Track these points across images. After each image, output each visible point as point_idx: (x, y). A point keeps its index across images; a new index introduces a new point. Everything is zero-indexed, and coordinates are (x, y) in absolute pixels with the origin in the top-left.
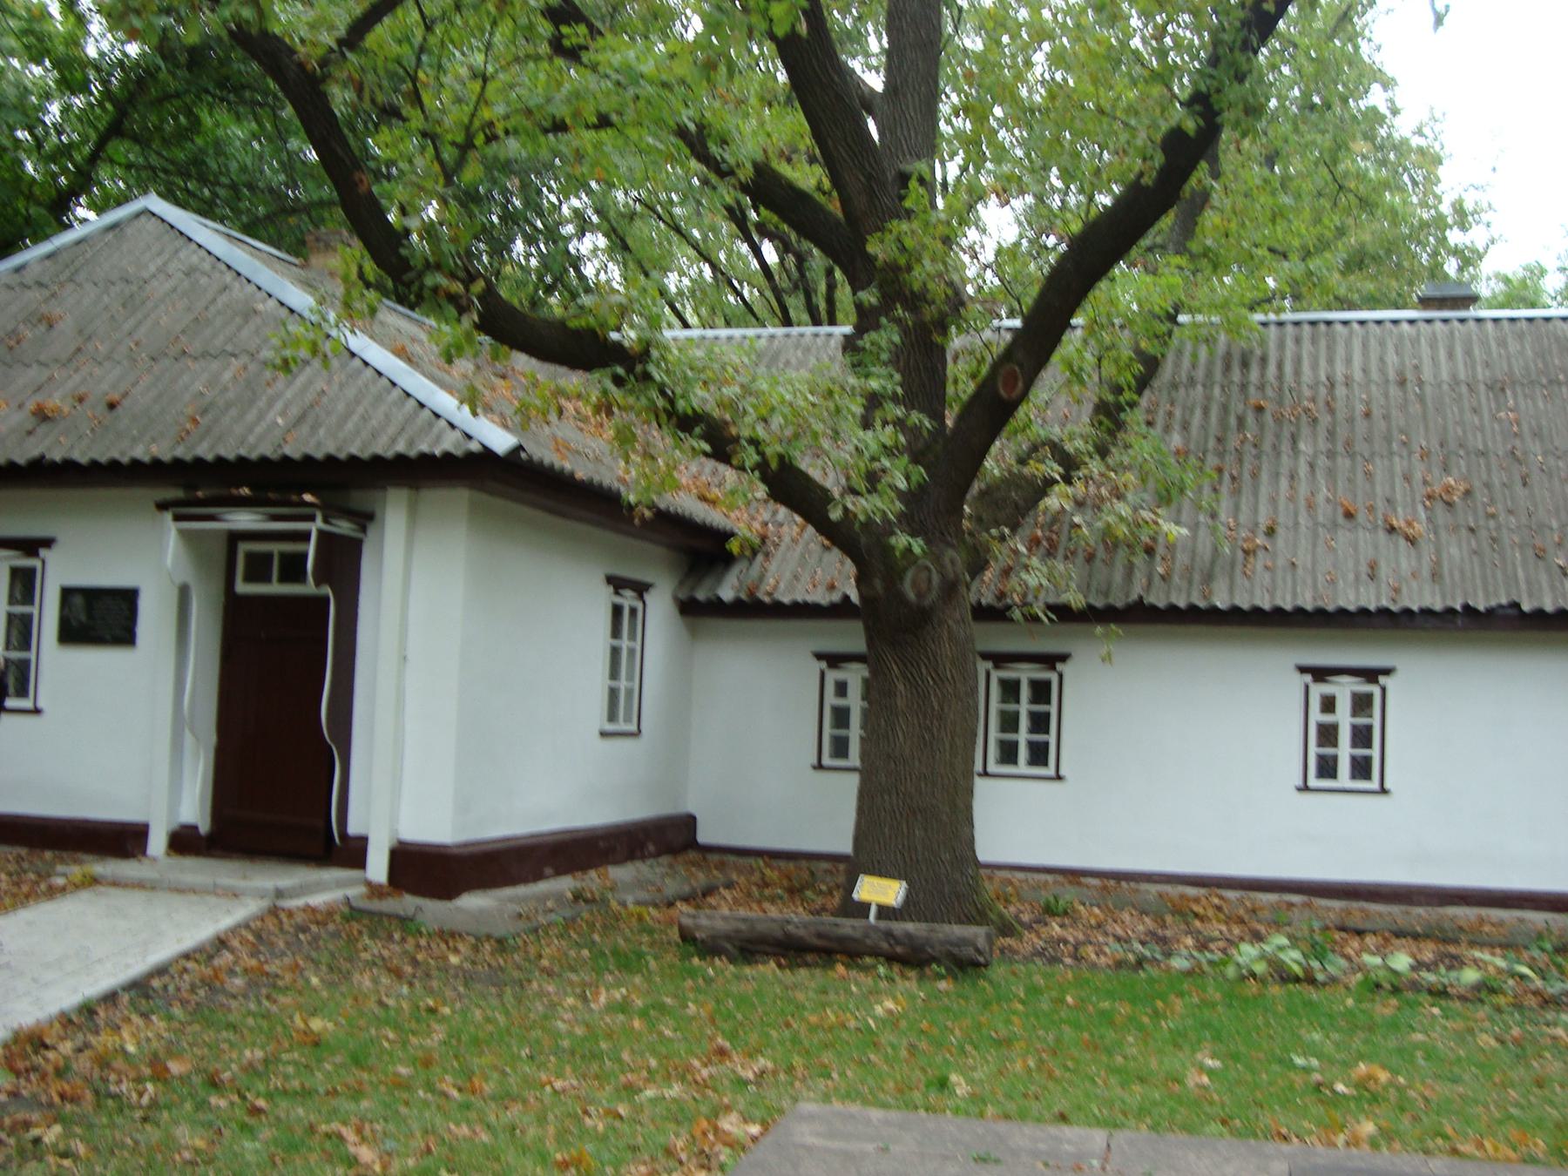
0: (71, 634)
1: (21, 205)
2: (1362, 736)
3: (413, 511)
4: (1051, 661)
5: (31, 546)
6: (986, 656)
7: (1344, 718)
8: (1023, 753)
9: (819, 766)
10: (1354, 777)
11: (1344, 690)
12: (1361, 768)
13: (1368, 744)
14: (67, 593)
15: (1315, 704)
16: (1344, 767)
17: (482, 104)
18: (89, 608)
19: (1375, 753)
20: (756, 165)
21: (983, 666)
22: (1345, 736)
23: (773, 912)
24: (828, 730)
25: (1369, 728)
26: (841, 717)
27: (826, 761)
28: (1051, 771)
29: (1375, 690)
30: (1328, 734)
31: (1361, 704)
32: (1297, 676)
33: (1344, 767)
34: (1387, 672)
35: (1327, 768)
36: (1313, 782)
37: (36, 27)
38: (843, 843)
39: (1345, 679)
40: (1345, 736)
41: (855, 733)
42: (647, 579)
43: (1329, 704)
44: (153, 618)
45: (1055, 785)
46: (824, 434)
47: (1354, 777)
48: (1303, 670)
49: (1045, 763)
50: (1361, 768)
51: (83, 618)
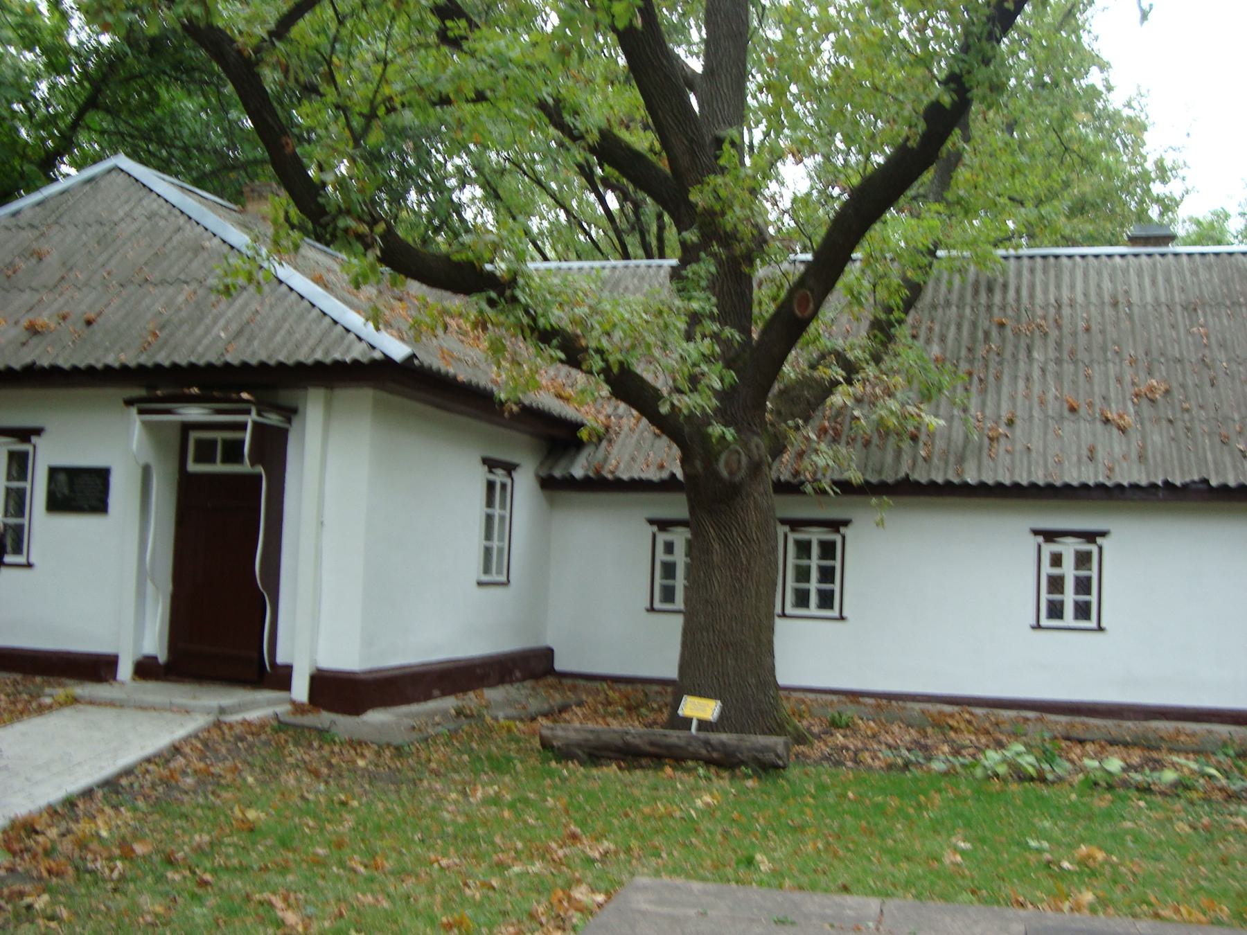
0: (57, 504)
1: (16, 163)
2: (1083, 585)
3: (328, 407)
4: (836, 525)
5: (25, 434)
6: (784, 522)
7: (1069, 571)
8: (814, 599)
9: (652, 609)
10: (1077, 617)
11: (1069, 548)
12: (1083, 611)
13: (1088, 591)
14: (53, 472)
15: (1046, 560)
16: (1069, 610)
17: (383, 83)
18: (71, 483)
19: (1093, 598)
20: (601, 131)
21: (782, 530)
22: (1069, 585)
23: (615, 725)
24: (658, 581)
25: (1089, 579)
26: (669, 570)
27: (657, 605)
28: (836, 613)
29: (1094, 549)
30: (1056, 584)
31: (1083, 560)
32: (1031, 538)
33: (1069, 610)
34: (1103, 534)
35: (1056, 611)
36: (1044, 622)
37: (29, 21)
38: (670, 670)
39: (1070, 540)
40: (1069, 585)
41: (680, 582)
42: (515, 460)
43: (1057, 560)
44: (122, 491)
45: (839, 624)
46: (656, 345)
47: (1077, 617)
48: (1036, 532)
49: (831, 607)
50: (1083, 611)
51: (66, 491)
